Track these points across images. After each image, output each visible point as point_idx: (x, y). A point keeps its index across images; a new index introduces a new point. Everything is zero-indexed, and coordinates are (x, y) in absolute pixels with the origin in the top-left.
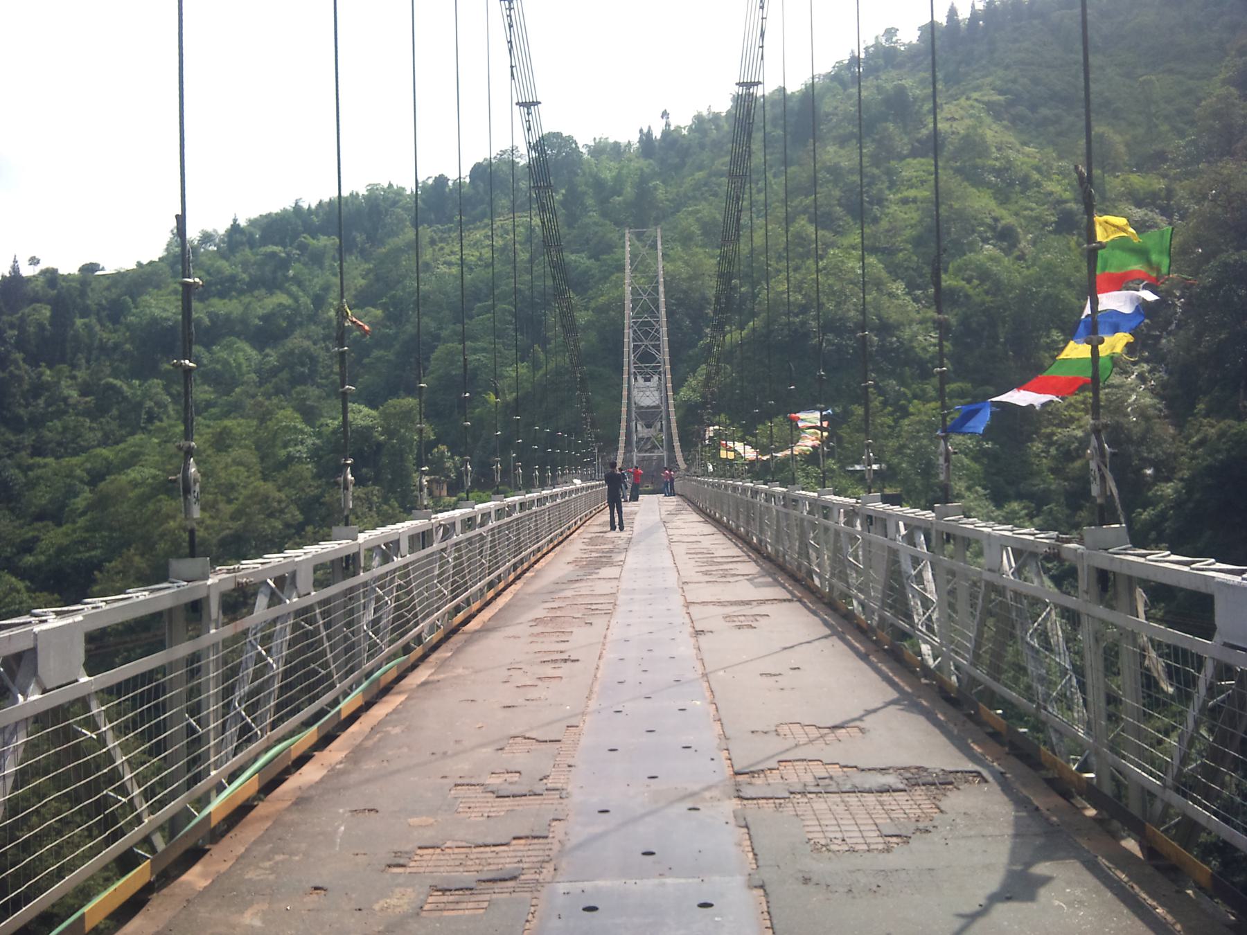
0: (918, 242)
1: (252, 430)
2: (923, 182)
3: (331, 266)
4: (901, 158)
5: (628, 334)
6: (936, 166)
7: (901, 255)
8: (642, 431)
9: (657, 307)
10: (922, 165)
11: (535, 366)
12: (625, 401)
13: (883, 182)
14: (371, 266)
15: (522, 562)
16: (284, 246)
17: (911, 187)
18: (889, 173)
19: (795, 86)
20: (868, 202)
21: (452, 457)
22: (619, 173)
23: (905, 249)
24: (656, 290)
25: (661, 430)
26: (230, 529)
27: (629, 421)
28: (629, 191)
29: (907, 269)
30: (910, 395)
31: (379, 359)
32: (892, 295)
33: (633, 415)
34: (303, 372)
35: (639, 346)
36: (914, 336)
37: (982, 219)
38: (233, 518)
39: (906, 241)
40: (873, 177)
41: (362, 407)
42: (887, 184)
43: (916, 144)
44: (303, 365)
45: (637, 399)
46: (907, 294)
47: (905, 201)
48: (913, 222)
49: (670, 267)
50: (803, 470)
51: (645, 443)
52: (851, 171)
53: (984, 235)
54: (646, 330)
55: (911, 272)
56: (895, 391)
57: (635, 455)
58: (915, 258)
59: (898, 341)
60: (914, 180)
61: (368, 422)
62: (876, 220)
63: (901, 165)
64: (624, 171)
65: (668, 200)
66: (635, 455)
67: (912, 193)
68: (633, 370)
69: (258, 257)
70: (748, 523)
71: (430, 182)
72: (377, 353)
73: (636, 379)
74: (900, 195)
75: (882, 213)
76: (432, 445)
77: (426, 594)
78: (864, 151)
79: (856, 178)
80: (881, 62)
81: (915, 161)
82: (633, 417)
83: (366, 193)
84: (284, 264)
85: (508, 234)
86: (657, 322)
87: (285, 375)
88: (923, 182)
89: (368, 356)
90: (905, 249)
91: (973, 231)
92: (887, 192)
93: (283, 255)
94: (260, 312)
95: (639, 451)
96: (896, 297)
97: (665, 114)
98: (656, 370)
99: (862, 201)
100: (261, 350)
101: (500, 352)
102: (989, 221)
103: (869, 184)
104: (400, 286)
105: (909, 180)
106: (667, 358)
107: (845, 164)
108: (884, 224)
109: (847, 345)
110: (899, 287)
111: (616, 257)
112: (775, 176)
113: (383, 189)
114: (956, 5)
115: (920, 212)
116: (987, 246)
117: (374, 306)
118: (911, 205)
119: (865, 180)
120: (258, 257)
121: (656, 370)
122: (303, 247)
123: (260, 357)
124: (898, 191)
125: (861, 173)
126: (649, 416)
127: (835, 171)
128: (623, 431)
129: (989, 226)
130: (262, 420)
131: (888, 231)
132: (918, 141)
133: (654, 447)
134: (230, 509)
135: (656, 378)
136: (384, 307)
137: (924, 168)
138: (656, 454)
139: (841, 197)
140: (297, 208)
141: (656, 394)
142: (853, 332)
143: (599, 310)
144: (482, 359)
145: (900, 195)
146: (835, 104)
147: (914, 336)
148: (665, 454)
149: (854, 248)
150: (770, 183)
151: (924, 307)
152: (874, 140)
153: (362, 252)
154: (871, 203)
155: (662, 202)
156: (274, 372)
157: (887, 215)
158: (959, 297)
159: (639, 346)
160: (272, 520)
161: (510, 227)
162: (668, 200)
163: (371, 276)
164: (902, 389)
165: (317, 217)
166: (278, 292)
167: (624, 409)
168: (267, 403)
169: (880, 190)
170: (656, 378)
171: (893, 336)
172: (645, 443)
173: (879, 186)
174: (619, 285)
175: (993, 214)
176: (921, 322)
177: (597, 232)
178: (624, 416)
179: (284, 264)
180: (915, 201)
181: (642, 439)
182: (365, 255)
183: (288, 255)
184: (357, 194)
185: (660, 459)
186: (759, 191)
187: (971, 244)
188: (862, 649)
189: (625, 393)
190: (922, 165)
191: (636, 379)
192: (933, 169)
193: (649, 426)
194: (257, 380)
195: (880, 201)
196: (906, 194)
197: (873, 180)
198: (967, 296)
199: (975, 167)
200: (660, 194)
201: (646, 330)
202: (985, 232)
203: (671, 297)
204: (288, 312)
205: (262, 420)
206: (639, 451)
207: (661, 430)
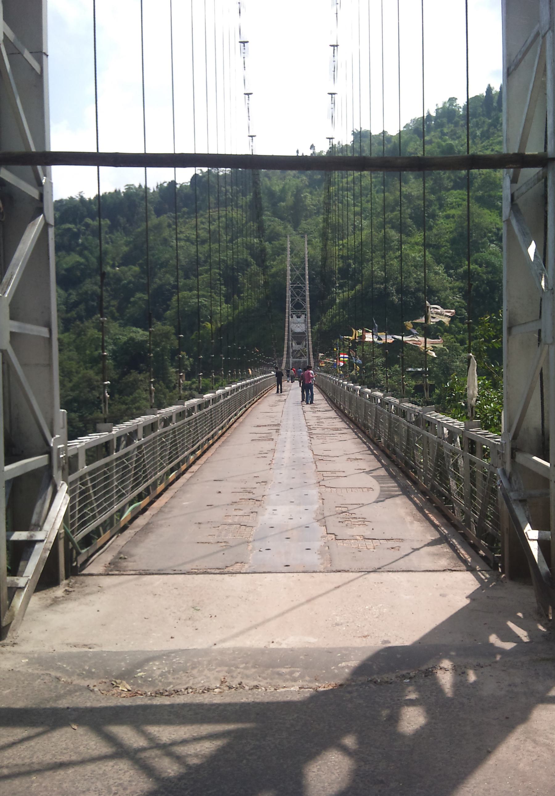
0: (453, 242)
1: (72, 340)
2: (459, 205)
3: (105, 237)
4: (448, 190)
5: (289, 294)
6: (468, 195)
7: (443, 249)
8: (295, 346)
9: (305, 279)
10: (460, 194)
11: (235, 307)
12: (287, 329)
13: (436, 205)
14: (132, 239)
15: (251, 401)
16: (75, 224)
17: (453, 208)
18: (439, 199)
19: (393, 132)
20: (427, 217)
21: (188, 359)
22: (284, 187)
23: (445, 246)
24: (304, 269)
25: (305, 346)
26: (71, 396)
27: (288, 340)
28: (290, 199)
29: (446, 258)
30: (443, 330)
31: (140, 298)
32: (436, 273)
33: (290, 338)
34: (93, 305)
35: (294, 300)
36: (447, 297)
37: (490, 229)
38: (72, 390)
39: (447, 241)
40: (431, 202)
41: (139, 330)
42: (438, 206)
43: (458, 180)
44: (93, 300)
45: (293, 329)
46: (445, 273)
47: (448, 217)
48: (451, 230)
49: (312, 252)
50: (382, 370)
51: (297, 353)
52: (418, 198)
53: (491, 238)
54: (298, 290)
55: (448, 259)
56: (435, 328)
57: (291, 360)
58: (451, 252)
59: (438, 299)
60: (454, 204)
61: (144, 338)
62: (431, 228)
63: (447, 194)
64: (287, 187)
65: (313, 205)
66: (291, 360)
67: (452, 212)
68: (290, 313)
69: (60, 231)
70: (350, 408)
71: (165, 185)
72: (138, 295)
73: (292, 317)
74: (445, 213)
75: (434, 223)
76: (177, 352)
77: (164, 440)
78: (427, 185)
79: (421, 202)
80: (445, 120)
81: (455, 192)
82: (290, 339)
83: (125, 191)
84: (76, 236)
85: (215, 221)
86: (304, 286)
87: (82, 307)
88: (459, 205)
89: (133, 297)
90: (445, 246)
91: (485, 236)
92: (437, 211)
93: (75, 230)
94: (65, 266)
95: (294, 358)
96: (439, 274)
97: (312, 147)
98: (304, 313)
99: (424, 216)
100: (66, 290)
101: (213, 298)
102: (494, 230)
103: (428, 206)
104: (242, 301)
105: (451, 204)
106: (309, 306)
107: (415, 193)
108: (435, 231)
109: (410, 301)
110: (440, 269)
111: (281, 242)
112: (377, 192)
113: (135, 188)
114: (492, 86)
115: (455, 224)
116: (492, 245)
117: (134, 265)
118: (451, 219)
119: (427, 203)
120: (60, 231)
121: (304, 313)
122: (87, 226)
123: (66, 295)
124: (445, 210)
125: (424, 199)
126: (299, 337)
127: (409, 197)
128: (286, 345)
129: (495, 233)
130: (79, 335)
131: (436, 235)
132: (460, 178)
133: (302, 356)
134: (71, 385)
135: (303, 316)
136: (141, 266)
137: (460, 196)
138: (303, 360)
139: (412, 213)
140: (82, 199)
141: (303, 325)
142: (413, 293)
143: (273, 276)
144: (203, 301)
145: (445, 213)
146: (416, 147)
147: (447, 297)
148: (307, 359)
149: (417, 244)
150: (374, 197)
151: (454, 280)
152: (432, 179)
153: (124, 229)
154: (428, 217)
155: (309, 206)
156: (76, 305)
157: (437, 225)
158: (474, 274)
159: (294, 300)
160: (93, 391)
161: (216, 217)
162: (313, 205)
163: (131, 245)
164: (439, 327)
165: (95, 205)
166: (73, 253)
167: (286, 333)
168: (81, 325)
169: (434, 210)
170: (303, 316)
171: (435, 296)
172: (297, 353)
173: (433, 207)
174: (283, 262)
175: (497, 226)
176: (451, 289)
177: (270, 225)
178: (286, 337)
179: (76, 236)
180: (453, 217)
181: (295, 351)
182: (127, 233)
183: (78, 230)
184: (119, 191)
185: (305, 362)
186: (368, 202)
187: (483, 243)
188: (436, 522)
189: (287, 325)
190: (460, 194)
191: (292, 317)
192: (466, 197)
193: (298, 343)
194: (65, 309)
195: (433, 216)
196: (448, 212)
197: (431, 203)
198: (478, 274)
199: (490, 196)
200: (308, 201)
201: (298, 290)
202: (492, 236)
203: (313, 270)
204: (83, 267)
205: (79, 335)
206: (294, 358)
207: (305, 346)
